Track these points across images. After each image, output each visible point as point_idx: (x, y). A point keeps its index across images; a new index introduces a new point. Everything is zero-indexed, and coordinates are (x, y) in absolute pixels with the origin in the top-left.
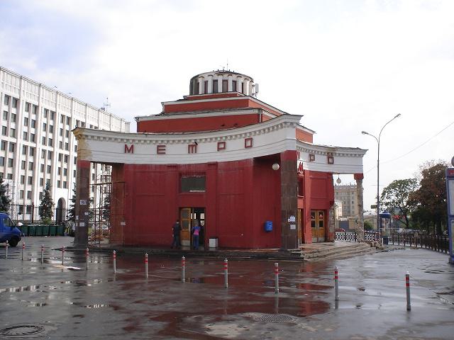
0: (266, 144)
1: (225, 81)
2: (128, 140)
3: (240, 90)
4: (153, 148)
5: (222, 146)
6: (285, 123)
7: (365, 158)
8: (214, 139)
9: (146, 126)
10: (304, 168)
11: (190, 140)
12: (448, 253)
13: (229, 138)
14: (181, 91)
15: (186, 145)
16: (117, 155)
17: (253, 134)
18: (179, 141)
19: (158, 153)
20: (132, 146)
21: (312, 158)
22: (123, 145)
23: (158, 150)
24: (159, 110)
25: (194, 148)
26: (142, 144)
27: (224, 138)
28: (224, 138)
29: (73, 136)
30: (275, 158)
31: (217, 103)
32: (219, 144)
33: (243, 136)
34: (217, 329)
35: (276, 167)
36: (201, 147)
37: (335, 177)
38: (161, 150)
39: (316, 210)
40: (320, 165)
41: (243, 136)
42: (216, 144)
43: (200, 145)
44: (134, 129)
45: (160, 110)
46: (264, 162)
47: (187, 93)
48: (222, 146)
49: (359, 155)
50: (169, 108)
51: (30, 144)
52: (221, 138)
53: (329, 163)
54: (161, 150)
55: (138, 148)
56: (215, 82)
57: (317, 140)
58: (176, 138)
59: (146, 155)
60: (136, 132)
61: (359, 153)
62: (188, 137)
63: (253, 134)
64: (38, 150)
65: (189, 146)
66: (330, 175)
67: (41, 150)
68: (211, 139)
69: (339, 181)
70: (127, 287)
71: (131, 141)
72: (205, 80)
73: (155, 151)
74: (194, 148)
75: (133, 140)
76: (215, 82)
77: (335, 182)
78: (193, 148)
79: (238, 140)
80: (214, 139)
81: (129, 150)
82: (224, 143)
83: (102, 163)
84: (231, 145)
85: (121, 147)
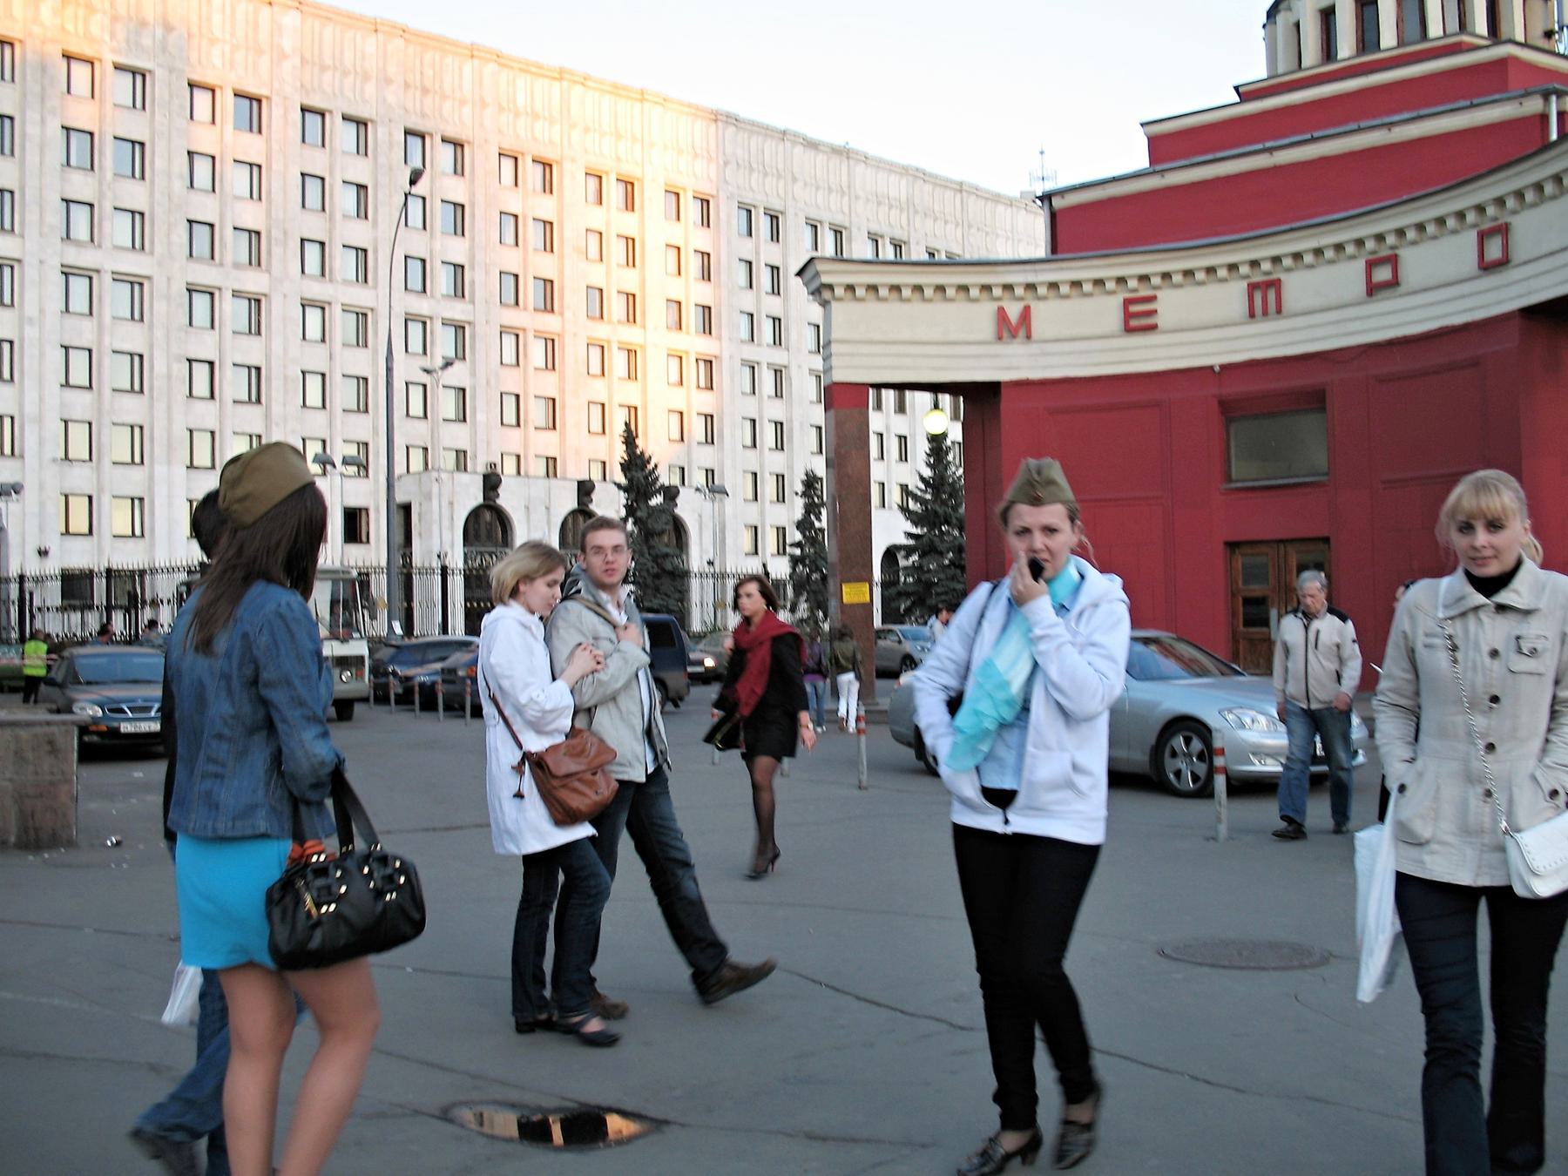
2: (1008, 288)
3: (1481, 26)
5: (1382, 274)
8: (1350, 249)
9: (1084, 224)
12: (356, 635)
13: (1411, 235)
15: (1238, 289)
17: (1511, 203)
20: (1026, 312)
22: (987, 309)
23: (1128, 316)
24: (1129, 155)
25: (1271, 295)
27: (1391, 240)
28: (1391, 240)
29: (795, 287)
32: (1371, 265)
38: (1138, 319)
41: (1471, 217)
42: (1360, 265)
44: (1033, 236)
45: (1140, 159)
47: (1256, 70)
48: (1382, 274)
50: (1167, 144)
51: (767, 355)
52: (1380, 238)
55: (1047, 316)
59: (1077, 338)
63: (1511, 203)
65: (1252, 288)
70: (1362, 804)
74: (1271, 295)
81: (1013, 329)
82: (1393, 260)
83: (935, 388)
85: (981, 316)
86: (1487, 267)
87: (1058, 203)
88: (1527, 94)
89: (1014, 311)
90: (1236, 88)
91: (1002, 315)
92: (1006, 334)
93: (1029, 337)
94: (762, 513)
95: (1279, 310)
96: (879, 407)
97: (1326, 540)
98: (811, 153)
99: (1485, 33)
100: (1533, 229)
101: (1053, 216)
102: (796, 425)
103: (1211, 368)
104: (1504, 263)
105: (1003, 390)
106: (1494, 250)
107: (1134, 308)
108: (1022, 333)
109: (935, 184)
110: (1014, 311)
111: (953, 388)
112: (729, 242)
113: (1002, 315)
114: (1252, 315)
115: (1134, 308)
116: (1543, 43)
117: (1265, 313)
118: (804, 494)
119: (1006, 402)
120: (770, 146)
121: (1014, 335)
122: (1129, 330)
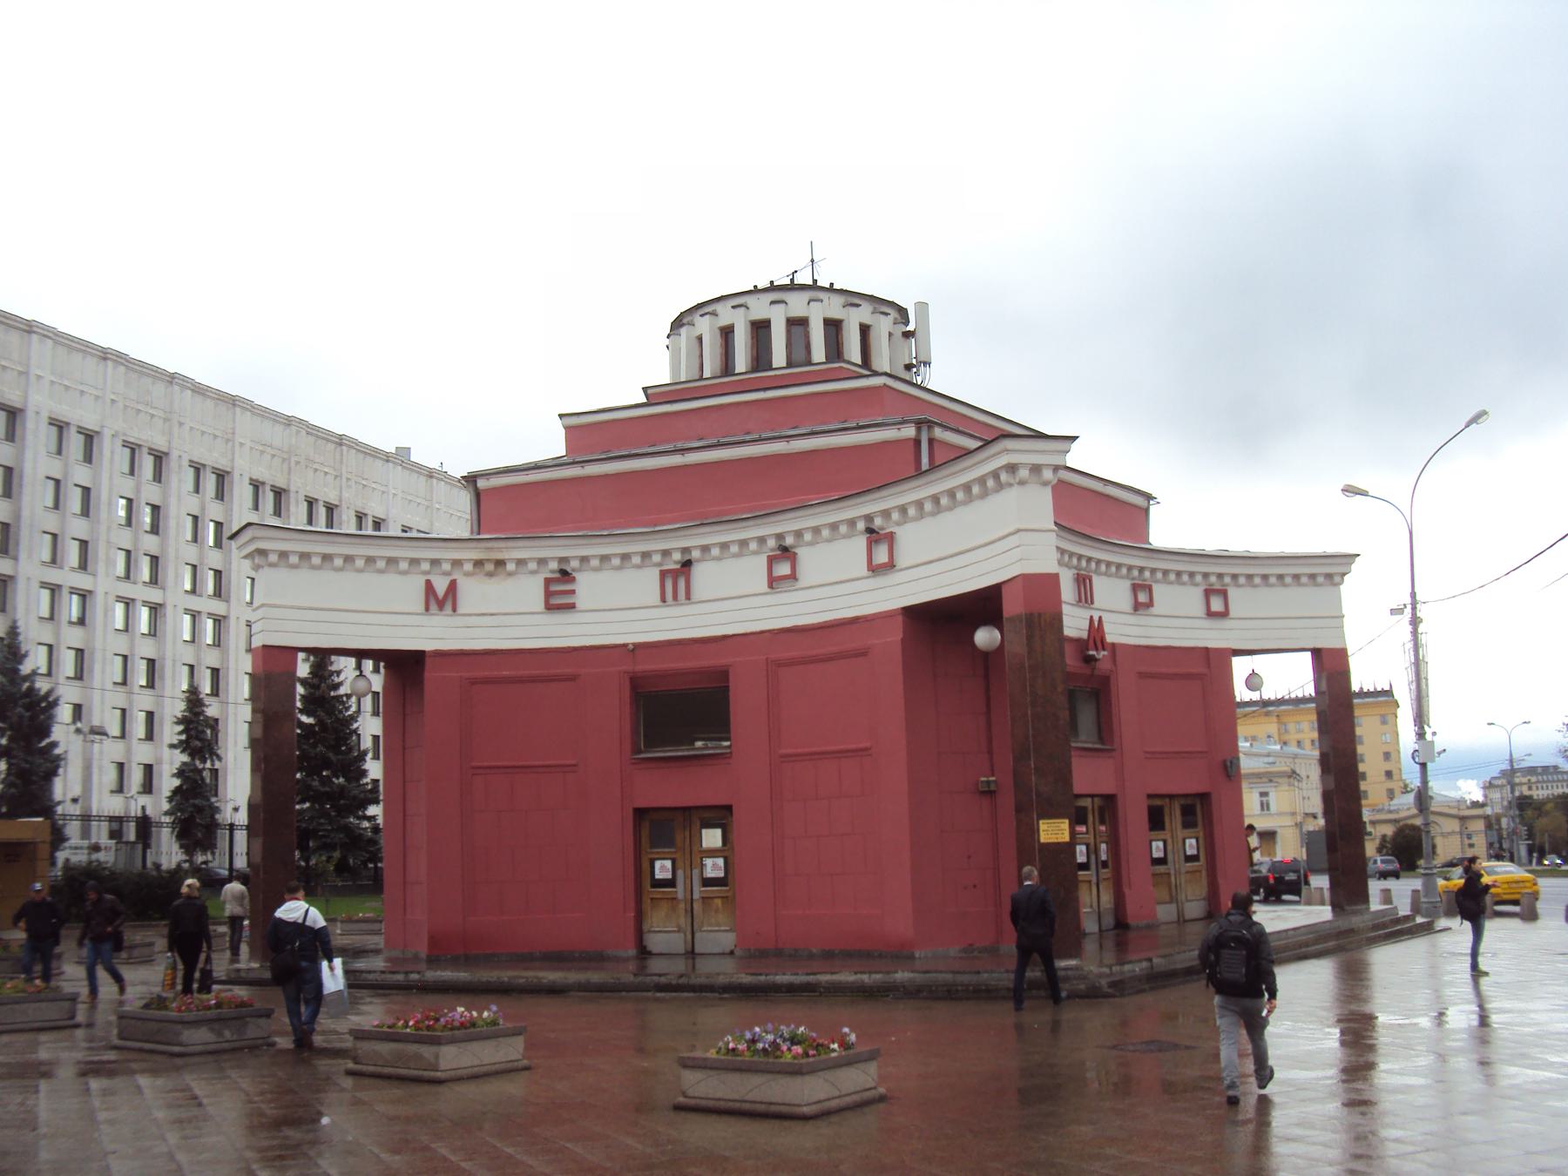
0: (962, 544)
1: (797, 325)
2: (435, 562)
4: (529, 590)
6: (1012, 468)
7: (1350, 589)
8: (753, 546)
9: (507, 505)
10: (1109, 639)
11: (666, 553)
14: (629, 365)
15: (653, 575)
16: (1188, 623)
17: (895, 516)
18: (605, 558)
19: (550, 607)
20: (453, 587)
21: (1142, 597)
22: (420, 582)
23: (548, 594)
26: (595, 570)
30: (983, 605)
31: (796, 397)
33: (657, 558)
34: (693, 1170)
35: (985, 637)
36: (705, 576)
37: (1241, 667)
38: (559, 592)
39: (1171, 797)
40: (1176, 622)
41: (657, 558)
43: (700, 572)
45: (554, 445)
46: (943, 623)
49: (1329, 576)
50: (589, 433)
53: (1210, 614)
54: (559, 592)
55: (474, 592)
56: (760, 329)
57: (1164, 532)
58: (733, 535)
59: (502, 615)
60: (466, 535)
61: (1325, 571)
62: (769, 529)
63: (895, 516)
64: (232, 621)
65: (663, 574)
66: (1214, 664)
67: (185, 463)
68: (743, 543)
69: (1253, 681)
71: (446, 567)
72: (724, 321)
73: (538, 603)
75: (457, 563)
76: (760, 329)
77: (1242, 693)
78: (678, 578)
79: (841, 546)
80: (753, 546)
81: (441, 600)
84: (815, 561)
86: (875, 569)
87: (481, 484)
88: (904, 422)
89: (441, 586)
90: (645, 389)
91: (429, 587)
92: (434, 607)
93: (454, 610)
94: (129, 751)
95: (688, 597)
96: (376, 738)
97: (729, 808)
98: (199, 399)
99: (859, 362)
100: (914, 540)
101: (478, 495)
102: (169, 663)
103: (625, 645)
104: (890, 566)
105: (428, 662)
106: (881, 556)
107: (554, 588)
108: (448, 607)
109: (56, 342)
110: (441, 586)
111: (377, 655)
112: (111, 478)
113: (429, 587)
114: (663, 600)
115: (554, 588)
116: (906, 376)
117: (675, 597)
118: (185, 746)
119: (431, 674)
120: (159, 389)
121: (441, 604)
122: (550, 607)
